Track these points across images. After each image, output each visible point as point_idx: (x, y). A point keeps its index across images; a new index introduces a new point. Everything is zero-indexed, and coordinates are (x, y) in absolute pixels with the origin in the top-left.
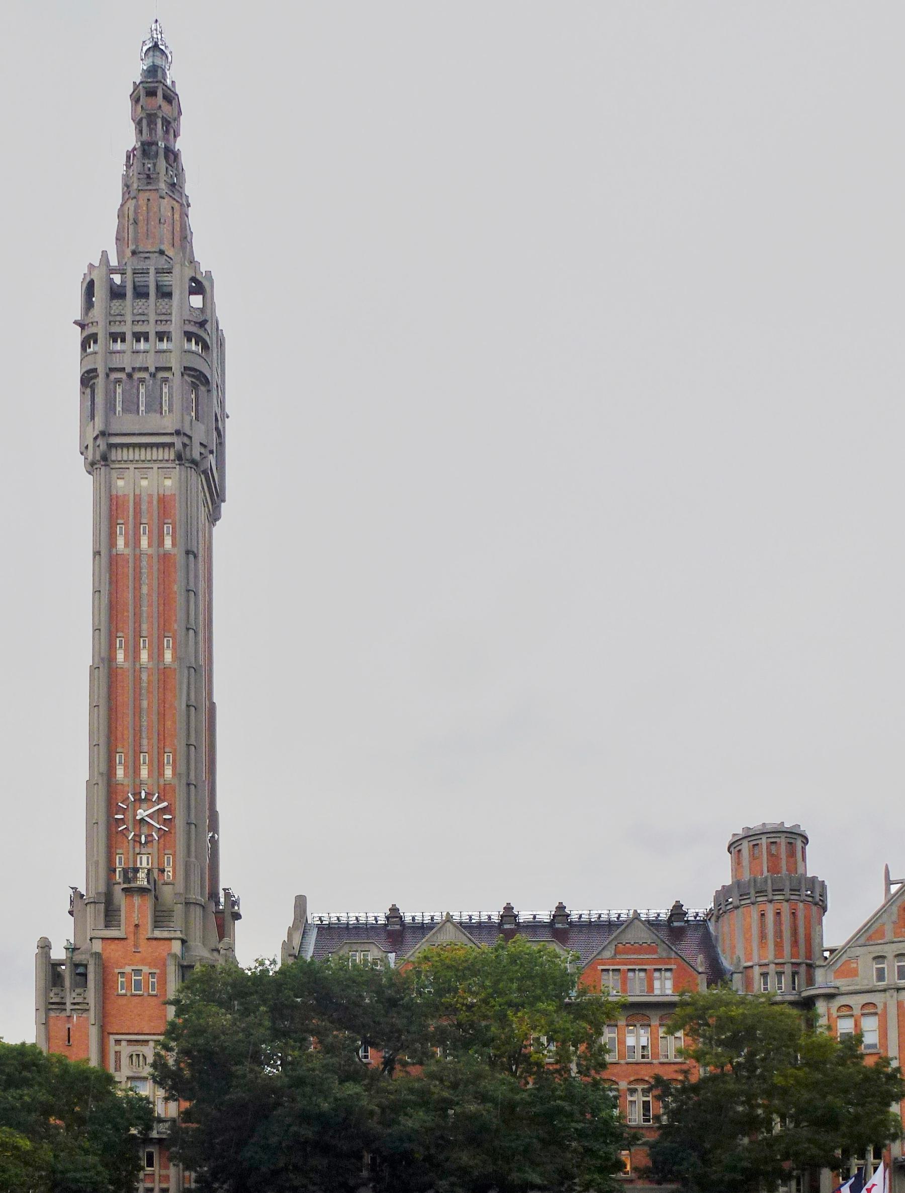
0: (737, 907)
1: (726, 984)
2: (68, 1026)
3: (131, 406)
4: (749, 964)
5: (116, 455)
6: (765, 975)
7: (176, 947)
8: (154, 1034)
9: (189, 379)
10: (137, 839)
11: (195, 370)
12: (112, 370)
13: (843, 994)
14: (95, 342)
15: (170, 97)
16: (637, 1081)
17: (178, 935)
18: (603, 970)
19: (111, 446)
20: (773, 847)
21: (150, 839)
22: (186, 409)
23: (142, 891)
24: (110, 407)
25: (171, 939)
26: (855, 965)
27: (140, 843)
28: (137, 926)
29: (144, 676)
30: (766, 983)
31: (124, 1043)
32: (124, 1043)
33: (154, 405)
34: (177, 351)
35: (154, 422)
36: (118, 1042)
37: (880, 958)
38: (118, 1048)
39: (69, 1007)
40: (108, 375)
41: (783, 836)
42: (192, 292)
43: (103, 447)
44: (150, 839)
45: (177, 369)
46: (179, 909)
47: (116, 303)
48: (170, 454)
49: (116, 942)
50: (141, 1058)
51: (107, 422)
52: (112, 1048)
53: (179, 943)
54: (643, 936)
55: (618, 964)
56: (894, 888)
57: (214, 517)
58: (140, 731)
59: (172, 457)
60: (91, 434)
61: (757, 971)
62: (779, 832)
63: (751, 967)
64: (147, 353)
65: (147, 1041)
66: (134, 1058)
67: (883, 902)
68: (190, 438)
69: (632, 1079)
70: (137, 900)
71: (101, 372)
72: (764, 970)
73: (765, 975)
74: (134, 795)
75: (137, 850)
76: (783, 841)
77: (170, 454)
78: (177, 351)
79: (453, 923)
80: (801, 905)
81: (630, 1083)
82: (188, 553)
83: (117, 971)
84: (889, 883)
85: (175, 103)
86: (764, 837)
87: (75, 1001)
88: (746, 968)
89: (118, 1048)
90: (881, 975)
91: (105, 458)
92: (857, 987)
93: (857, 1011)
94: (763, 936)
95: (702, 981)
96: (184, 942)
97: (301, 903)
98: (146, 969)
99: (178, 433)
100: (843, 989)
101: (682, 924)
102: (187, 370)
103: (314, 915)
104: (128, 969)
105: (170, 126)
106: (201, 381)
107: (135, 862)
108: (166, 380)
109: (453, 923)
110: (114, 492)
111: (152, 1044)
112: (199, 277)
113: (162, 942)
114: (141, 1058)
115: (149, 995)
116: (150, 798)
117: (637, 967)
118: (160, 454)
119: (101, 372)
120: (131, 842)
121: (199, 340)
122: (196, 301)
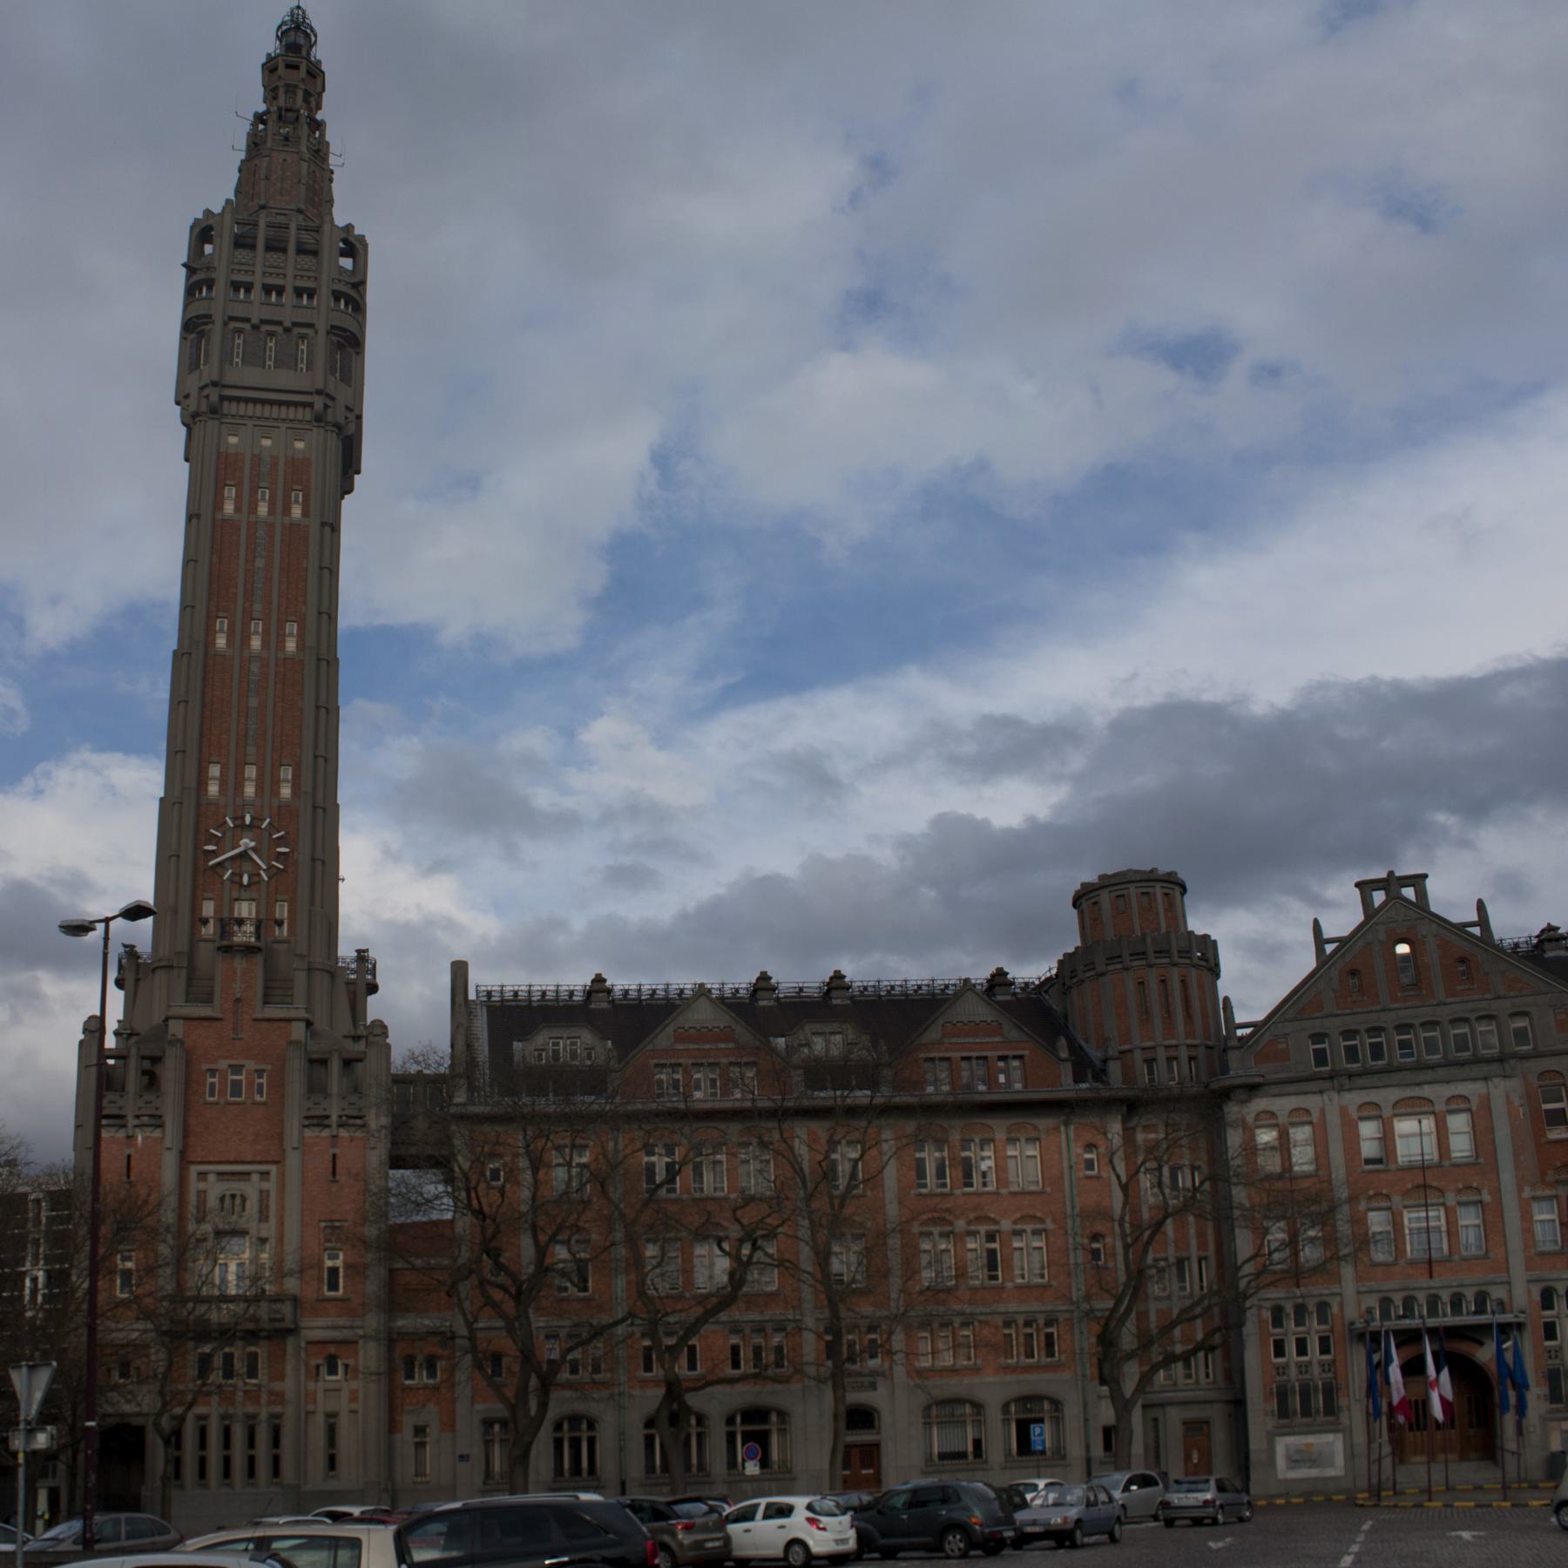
0: (1103, 974)
1: (1101, 1075)
2: (127, 1152)
3: (254, 358)
4: (1126, 1047)
5: (228, 408)
6: (1150, 1062)
7: (298, 1032)
8: (260, 1162)
9: (336, 339)
10: (236, 880)
11: (345, 330)
12: (232, 319)
13: (1270, 1084)
14: (210, 288)
15: (315, 73)
16: (1023, 1219)
17: (302, 1014)
18: (657, 1065)
19: (222, 398)
20: (1145, 898)
21: (256, 879)
22: (332, 370)
23: (249, 950)
24: (226, 358)
25: (289, 1020)
26: (1282, 1046)
27: (241, 884)
28: (238, 1000)
29: (255, 668)
30: (1151, 1072)
31: (212, 1178)
32: (212, 1178)
33: (287, 361)
34: (324, 312)
35: (284, 379)
36: (202, 1175)
37: (1318, 1037)
38: (202, 1186)
39: (131, 1121)
40: (226, 324)
41: (1158, 886)
42: (344, 254)
43: (214, 398)
44: (256, 879)
45: (322, 328)
46: (300, 979)
47: (242, 255)
48: (309, 414)
49: (206, 1024)
50: (238, 1201)
51: (221, 373)
52: (194, 1185)
53: (302, 1025)
54: (978, 1011)
55: (947, 1050)
56: (1329, 948)
57: (349, 489)
58: (246, 736)
59: (308, 417)
60: (193, 384)
61: (1138, 1055)
62: (1150, 878)
63: (1130, 1051)
64: (288, 309)
65: (249, 1174)
66: (228, 1202)
67: (1314, 965)
68: (333, 399)
69: (972, 1216)
70: (239, 964)
71: (218, 319)
72: (1149, 1055)
73: (1150, 1062)
74: (234, 819)
75: (235, 895)
76: (1159, 890)
77: (309, 414)
78: (324, 312)
79: (711, 999)
80: (1194, 972)
81: (1015, 1222)
82: (323, 524)
83: (205, 1067)
84: (1319, 939)
85: (319, 80)
86: (1132, 887)
87: (311, 1113)
88: (1121, 1052)
89: (202, 1186)
90: (1320, 1057)
91: (214, 411)
92: (1291, 1075)
93: (1440, 1107)
94: (1145, 1011)
95: (1067, 1072)
96: (309, 1024)
97: (459, 970)
98: (251, 1065)
99: (319, 392)
100: (1270, 1077)
101: (1008, 998)
102: (334, 329)
103: (482, 979)
104: (223, 1064)
105: (314, 98)
106: (350, 342)
107: (232, 909)
108: (303, 337)
109: (711, 999)
110: (223, 449)
111: (255, 1178)
112: (351, 239)
113: (276, 1024)
114: (238, 1201)
115: (255, 1103)
116: (256, 823)
117: (974, 1054)
118: (300, 413)
119: (218, 319)
120: (228, 885)
121: (350, 300)
122: (346, 263)
